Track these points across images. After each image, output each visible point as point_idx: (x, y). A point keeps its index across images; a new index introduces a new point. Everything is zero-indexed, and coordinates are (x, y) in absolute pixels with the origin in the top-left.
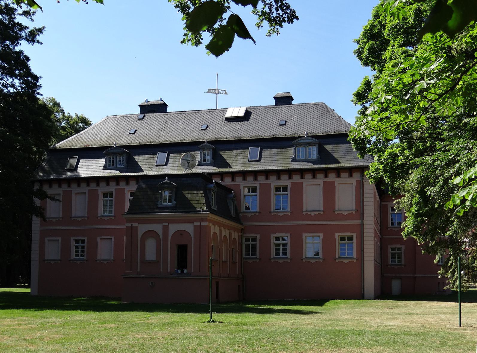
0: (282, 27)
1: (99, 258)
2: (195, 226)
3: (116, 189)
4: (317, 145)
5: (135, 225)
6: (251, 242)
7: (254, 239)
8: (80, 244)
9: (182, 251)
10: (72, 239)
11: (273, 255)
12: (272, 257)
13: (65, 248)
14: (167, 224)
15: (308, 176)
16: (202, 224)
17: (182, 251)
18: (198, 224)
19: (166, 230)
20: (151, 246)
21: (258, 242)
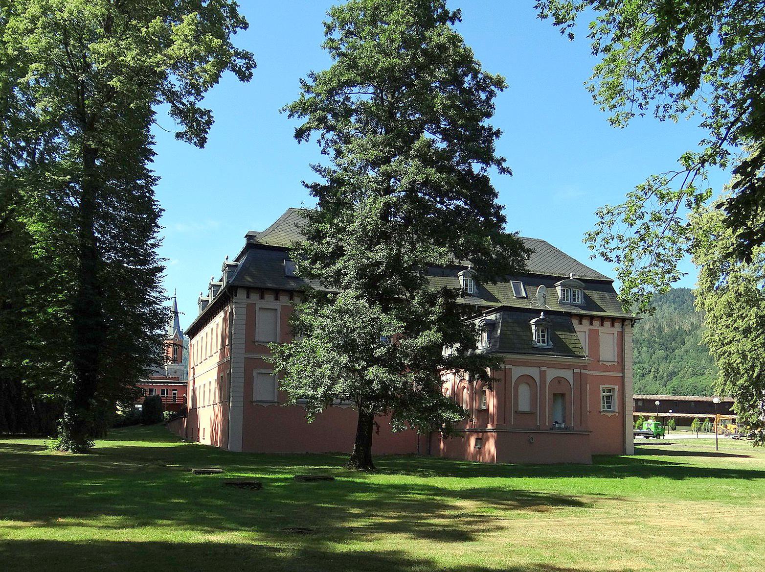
0: (290, 116)
10: (602, 387)
16: (583, 371)
18: (579, 371)
19: (543, 375)
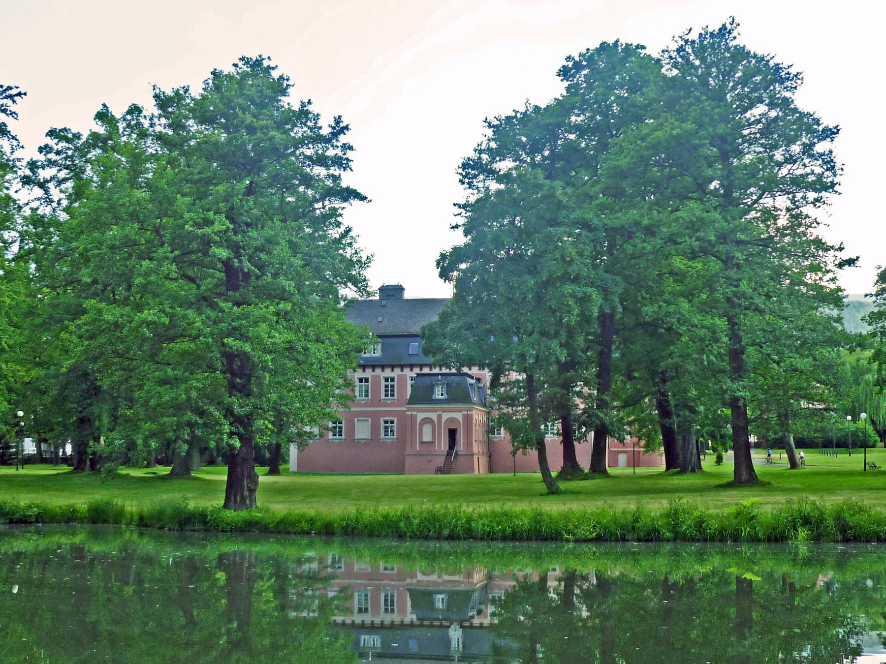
13: (375, 429)
19: (440, 417)
20: (427, 429)
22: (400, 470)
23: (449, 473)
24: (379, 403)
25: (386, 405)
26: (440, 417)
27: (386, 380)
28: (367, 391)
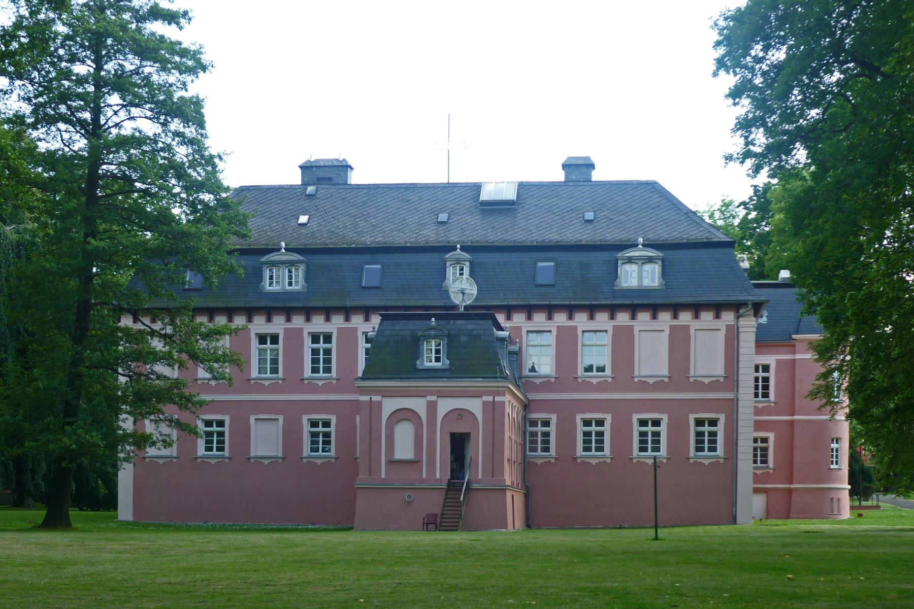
1: (253, 454)
2: (484, 403)
3: (285, 329)
4: (660, 262)
5: (376, 398)
6: (594, 428)
7: (546, 423)
8: (706, 429)
9: (459, 444)
11: (580, 451)
12: (578, 454)
13: (291, 436)
14: (434, 398)
15: (644, 317)
16: (498, 399)
17: (459, 444)
18: (490, 399)
19: (432, 408)
20: (404, 434)
21: (552, 429)
22: (346, 523)
23: (454, 528)
24: (301, 384)
25: (314, 389)
26: (432, 408)
27: (315, 338)
28: (275, 361)
